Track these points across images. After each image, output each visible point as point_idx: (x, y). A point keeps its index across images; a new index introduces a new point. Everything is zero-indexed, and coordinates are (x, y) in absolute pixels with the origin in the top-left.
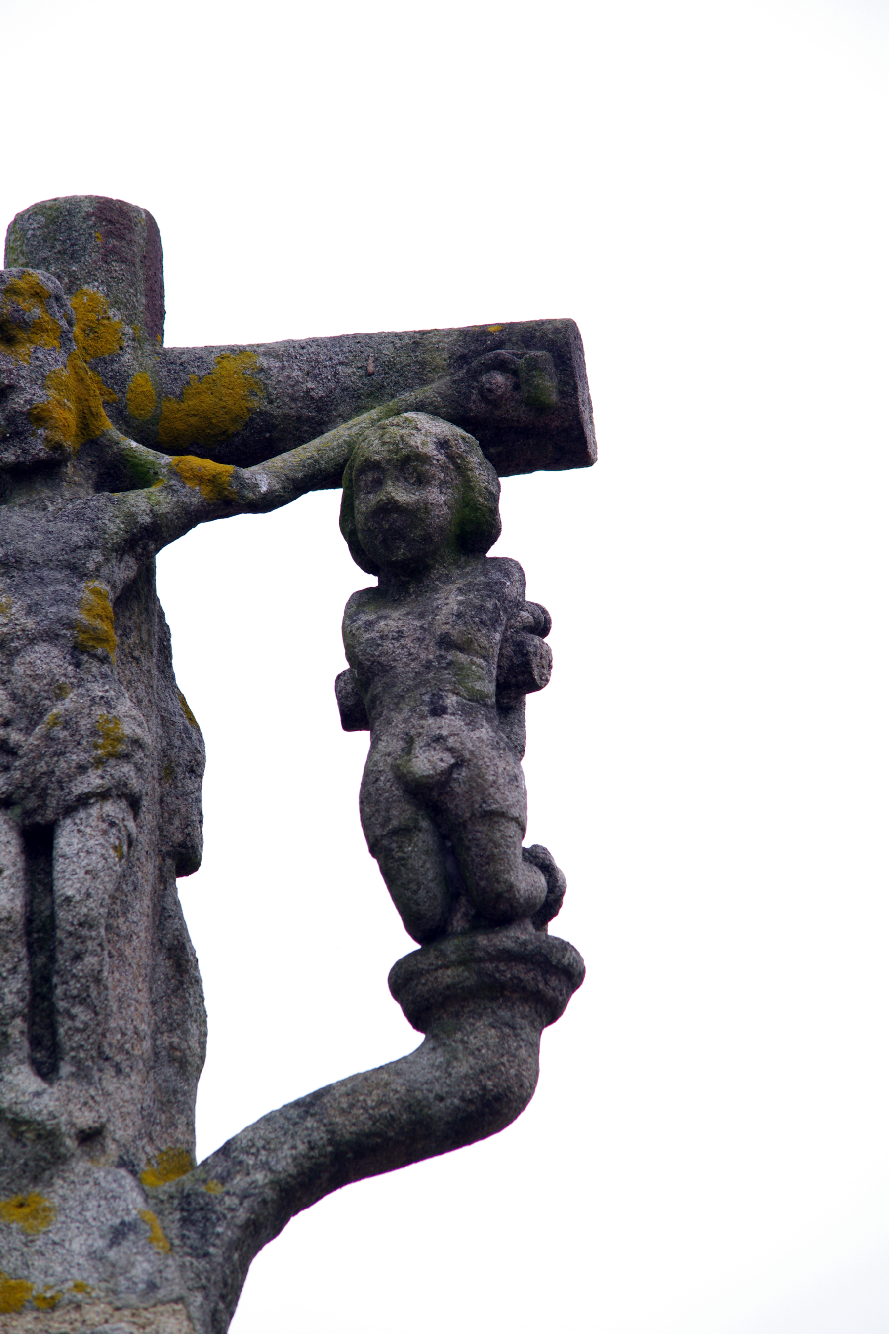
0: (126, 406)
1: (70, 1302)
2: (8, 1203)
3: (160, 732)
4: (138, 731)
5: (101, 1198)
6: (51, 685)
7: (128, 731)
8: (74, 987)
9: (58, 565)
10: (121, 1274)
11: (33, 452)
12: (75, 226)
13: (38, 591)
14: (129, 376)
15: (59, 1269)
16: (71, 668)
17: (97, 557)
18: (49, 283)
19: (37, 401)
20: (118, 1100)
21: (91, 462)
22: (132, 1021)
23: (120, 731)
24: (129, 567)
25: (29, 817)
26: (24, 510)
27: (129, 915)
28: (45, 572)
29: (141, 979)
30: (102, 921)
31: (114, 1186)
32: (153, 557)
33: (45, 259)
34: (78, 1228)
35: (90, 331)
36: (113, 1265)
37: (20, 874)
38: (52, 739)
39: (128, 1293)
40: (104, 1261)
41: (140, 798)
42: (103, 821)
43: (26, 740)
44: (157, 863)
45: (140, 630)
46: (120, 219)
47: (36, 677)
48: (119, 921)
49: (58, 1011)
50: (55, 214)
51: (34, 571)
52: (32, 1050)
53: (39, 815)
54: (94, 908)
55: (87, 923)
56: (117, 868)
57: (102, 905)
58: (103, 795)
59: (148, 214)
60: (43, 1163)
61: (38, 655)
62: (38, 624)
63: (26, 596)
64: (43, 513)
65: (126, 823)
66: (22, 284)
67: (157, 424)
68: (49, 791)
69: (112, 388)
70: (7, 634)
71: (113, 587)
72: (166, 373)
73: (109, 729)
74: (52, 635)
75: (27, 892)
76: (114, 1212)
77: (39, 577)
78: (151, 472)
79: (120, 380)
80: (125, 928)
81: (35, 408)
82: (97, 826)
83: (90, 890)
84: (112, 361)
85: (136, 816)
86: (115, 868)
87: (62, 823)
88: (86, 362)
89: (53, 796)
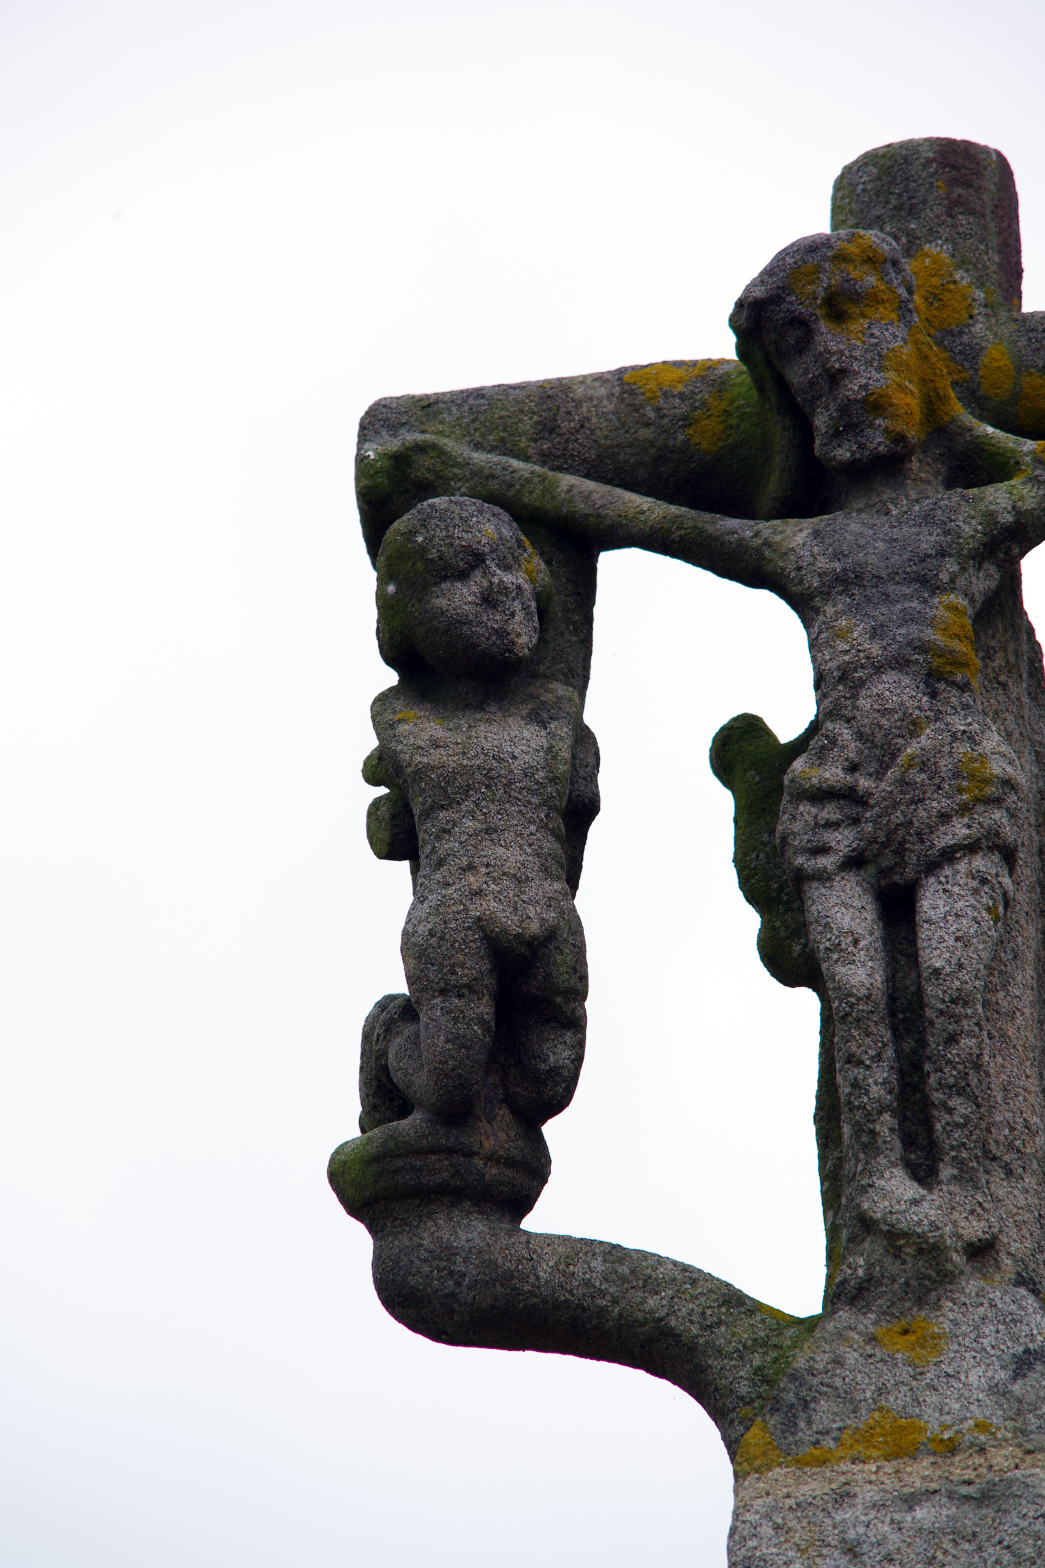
0: (979, 385)
1: (972, 1445)
2: (890, 1330)
3: (1036, 770)
4: (1009, 769)
5: (999, 1321)
6: (903, 720)
7: (997, 771)
8: (950, 1075)
9: (905, 579)
10: (1030, 1411)
11: (872, 446)
12: (912, 176)
13: (884, 610)
14: (982, 349)
15: (957, 1406)
16: (925, 699)
17: (951, 566)
18: (884, 245)
19: (873, 386)
20: (1011, 1207)
21: (940, 454)
22: (1021, 1113)
23: (988, 771)
24: (989, 576)
25: (885, 877)
26: (863, 515)
27: (1010, 989)
28: (891, 588)
29: (1028, 1064)
30: (979, 996)
31: (1014, 1307)
32: (1018, 563)
33: (878, 217)
34: (974, 1357)
35: (934, 298)
36: (1020, 1401)
37: (879, 944)
38: (908, 784)
39: (1040, 1433)
40: (1008, 1396)
41: (1016, 849)
42: (973, 878)
43: (877, 787)
44: (1040, 926)
45: (1005, 651)
46: (966, 163)
47: (885, 712)
48: (998, 996)
49: (933, 1104)
50: (889, 163)
51: (877, 587)
52: (905, 1151)
53: (897, 874)
54: (968, 981)
55: (960, 999)
56: (992, 933)
57: (977, 978)
58: (971, 848)
59: (999, 154)
60: (927, 1283)
61: (887, 686)
62: (885, 649)
63: (869, 616)
64: (886, 518)
65: (1000, 879)
66: (852, 249)
67: (1017, 404)
68: (908, 845)
69: (962, 365)
70: (849, 663)
71: (972, 601)
72: (1025, 343)
73: (974, 769)
74: (901, 661)
75: (887, 965)
76: (1016, 1339)
77: (884, 594)
78: (1012, 461)
79: (971, 354)
80: (1006, 1004)
81: (872, 394)
82: (967, 884)
83: (963, 960)
84: (961, 333)
85: (1011, 871)
86: (990, 933)
87: (924, 882)
88: (929, 335)
89: (912, 851)
